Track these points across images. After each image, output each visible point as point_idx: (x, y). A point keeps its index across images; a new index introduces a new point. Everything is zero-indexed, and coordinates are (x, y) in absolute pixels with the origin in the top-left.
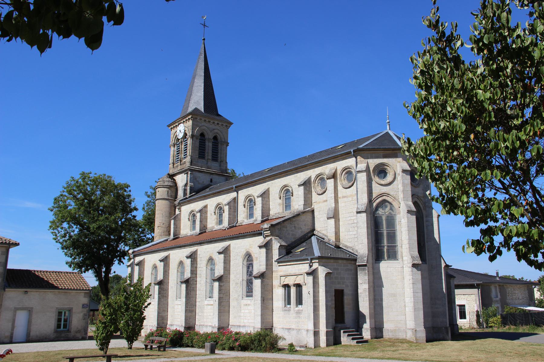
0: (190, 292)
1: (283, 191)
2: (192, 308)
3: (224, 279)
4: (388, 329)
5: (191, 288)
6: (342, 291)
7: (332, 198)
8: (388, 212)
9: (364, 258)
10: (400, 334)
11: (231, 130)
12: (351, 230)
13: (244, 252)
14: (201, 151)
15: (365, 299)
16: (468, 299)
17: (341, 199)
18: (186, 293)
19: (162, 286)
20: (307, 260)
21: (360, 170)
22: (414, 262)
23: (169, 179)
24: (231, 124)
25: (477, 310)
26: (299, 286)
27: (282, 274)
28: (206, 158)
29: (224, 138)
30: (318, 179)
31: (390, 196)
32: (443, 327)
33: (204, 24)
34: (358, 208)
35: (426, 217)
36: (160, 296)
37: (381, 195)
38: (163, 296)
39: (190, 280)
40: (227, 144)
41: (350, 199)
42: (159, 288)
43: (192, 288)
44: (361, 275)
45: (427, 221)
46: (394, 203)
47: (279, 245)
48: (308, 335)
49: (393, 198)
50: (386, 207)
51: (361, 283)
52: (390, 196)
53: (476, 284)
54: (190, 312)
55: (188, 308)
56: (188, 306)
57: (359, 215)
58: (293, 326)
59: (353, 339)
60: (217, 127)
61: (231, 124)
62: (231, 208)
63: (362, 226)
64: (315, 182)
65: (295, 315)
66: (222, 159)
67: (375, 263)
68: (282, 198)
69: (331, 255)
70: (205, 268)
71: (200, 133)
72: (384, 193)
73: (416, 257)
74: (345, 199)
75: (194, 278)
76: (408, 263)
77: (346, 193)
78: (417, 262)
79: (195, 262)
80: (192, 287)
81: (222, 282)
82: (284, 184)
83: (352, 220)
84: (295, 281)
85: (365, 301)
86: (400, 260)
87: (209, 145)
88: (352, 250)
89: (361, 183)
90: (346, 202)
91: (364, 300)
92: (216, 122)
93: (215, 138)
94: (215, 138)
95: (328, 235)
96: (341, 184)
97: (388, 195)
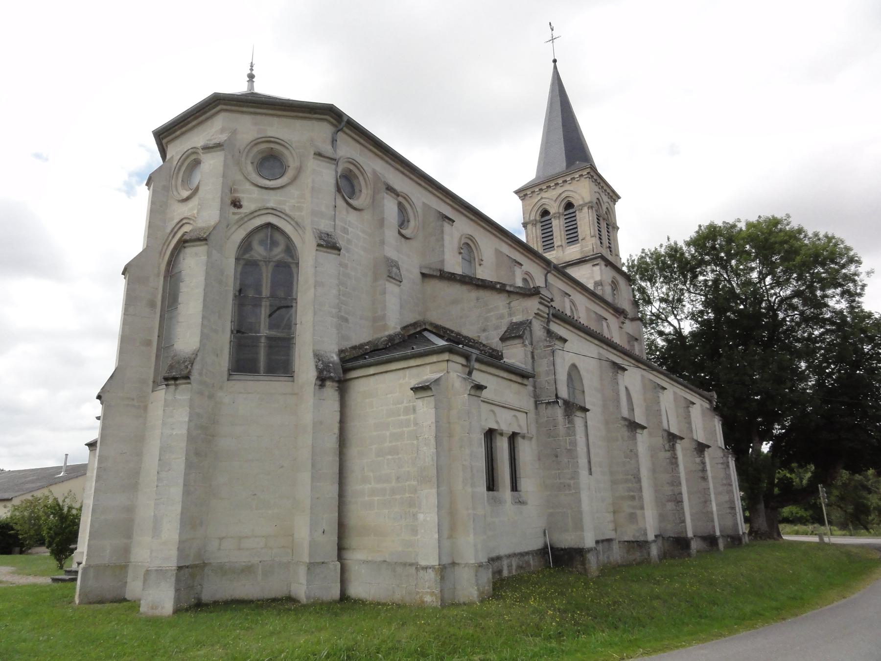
33: (554, 37)
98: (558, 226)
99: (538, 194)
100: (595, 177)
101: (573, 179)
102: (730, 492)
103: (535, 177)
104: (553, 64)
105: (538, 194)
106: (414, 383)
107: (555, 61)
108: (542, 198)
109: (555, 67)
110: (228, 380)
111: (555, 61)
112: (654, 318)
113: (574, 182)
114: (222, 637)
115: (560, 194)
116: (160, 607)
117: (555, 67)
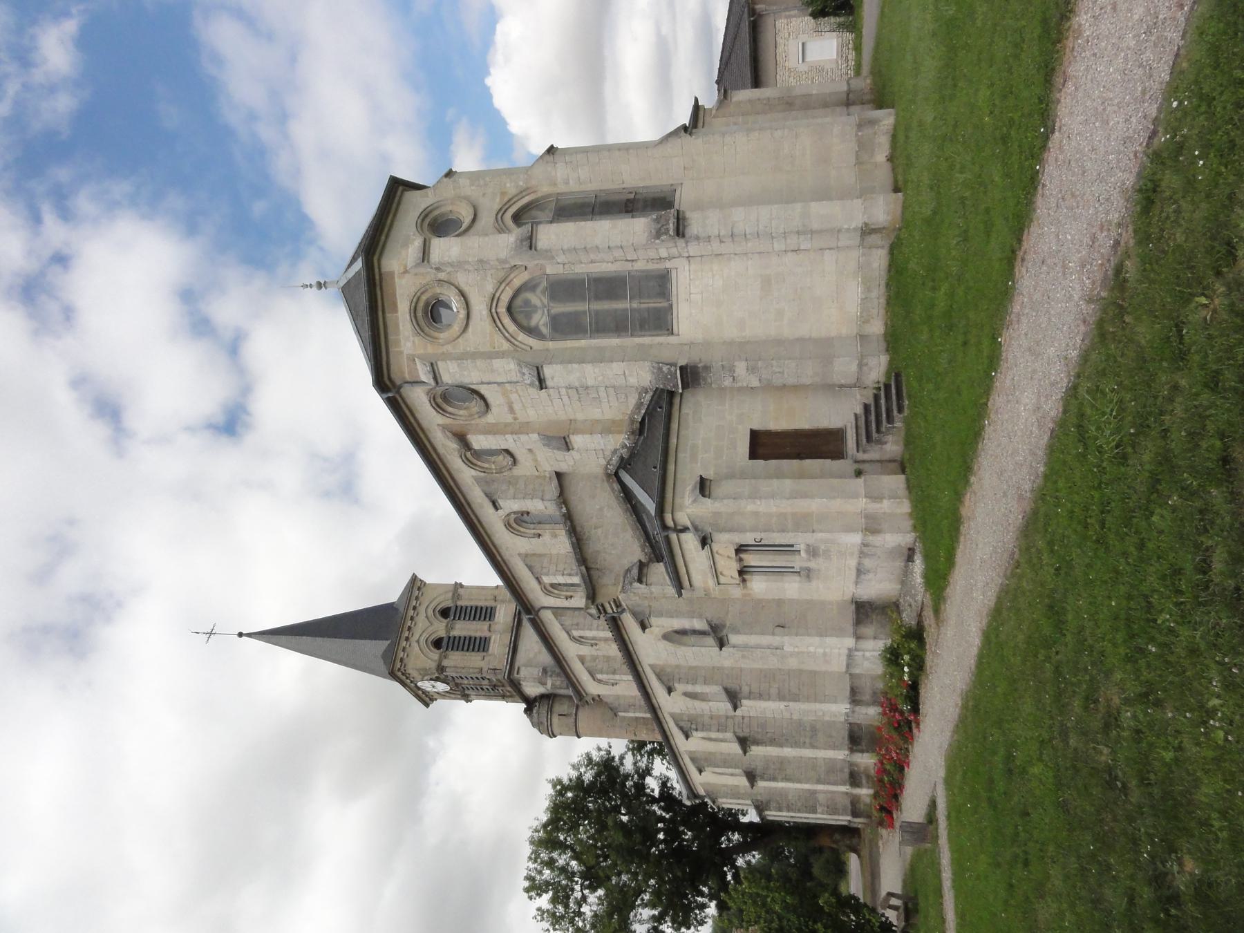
0: (769, 735)
1: (522, 530)
2: (805, 730)
3: (733, 685)
4: (862, 299)
5: (758, 732)
6: (755, 436)
7: (516, 438)
8: (543, 298)
9: (663, 372)
10: (876, 265)
11: (429, 578)
12: (595, 395)
13: (664, 645)
14: (471, 647)
15: (777, 370)
16: (786, 35)
17: (518, 415)
18: (771, 746)
19: (758, 772)
20: (668, 541)
21: (431, 376)
22: (671, 233)
23: (534, 711)
24: (414, 578)
25: (811, 15)
26: (740, 549)
27: (711, 583)
28: (487, 634)
29: (446, 592)
30: (479, 463)
31: (497, 295)
32: (856, 135)
33: (208, 635)
34: (531, 385)
35: (555, 184)
36: (780, 777)
37: (495, 319)
38: (780, 769)
39: (741, 735)
40: (458, 586)
41: (514, 397)
42: (763, 778)
43: (760, 730)
44: (709, 381)
45: (567, 183)
46: (517, 282)
47: (636, 585)
48: (878, 545)
49: (503, 285)
50: (527, 303)
51: (731, 379)
52: (497, 295)
53: (749, 17)
54: (816, 735)
55: (808, 741)
56: (802, 740)
57: (549, 383)
58: (853, 563)
59: (890, 419)
60: (422, 610)
61: (414, 578)
62: (577, 624)
63: (578, 374)
64: (487, 468)
65: (820, 560)
66: (489, 598)
67: (678, 335)
68: (539, 532)
69: (655, 468)
70: (711, 703)
71: (432, 649)
72: (490, 310)
73: (658, 223)
74: (517, 407)
75: (736, 723)
76: (676, 246)
77: (499, 405)
78: (671, 225)
79: (699, 720)
80: (756, 729)
81: (741, 689)
82: (504, 528)
83: (567, 392)
84: (728, 557)
85: (781, 370)
86: (668, 265)
87: (463, 629)
88: (646, 393)
89: (465, 373)
90: (523, 406)
91: (779, 372)
92: (411, 612)
93: (445, 613)
94: (445, 613)
95: (611, 447)
96: (480, 417)
97: (494, 300)
98: (463, 629)
99: (410, 645)
100: (409, 681)
101: (409, 628)
102: (754, 529)
103: (489, 81)
104: (244, 637)
105: (410, 645)
106: (640, 630)
107: (240, 635)
108: (418, 641)
109: (249, 635)
110: (678, 335)
111: (240, 635)
112: (539, 860)
113: (421, 599)
114: (1225, 451)
115: (427, 617)
116: (1215, 815)
117: (249, 635)
